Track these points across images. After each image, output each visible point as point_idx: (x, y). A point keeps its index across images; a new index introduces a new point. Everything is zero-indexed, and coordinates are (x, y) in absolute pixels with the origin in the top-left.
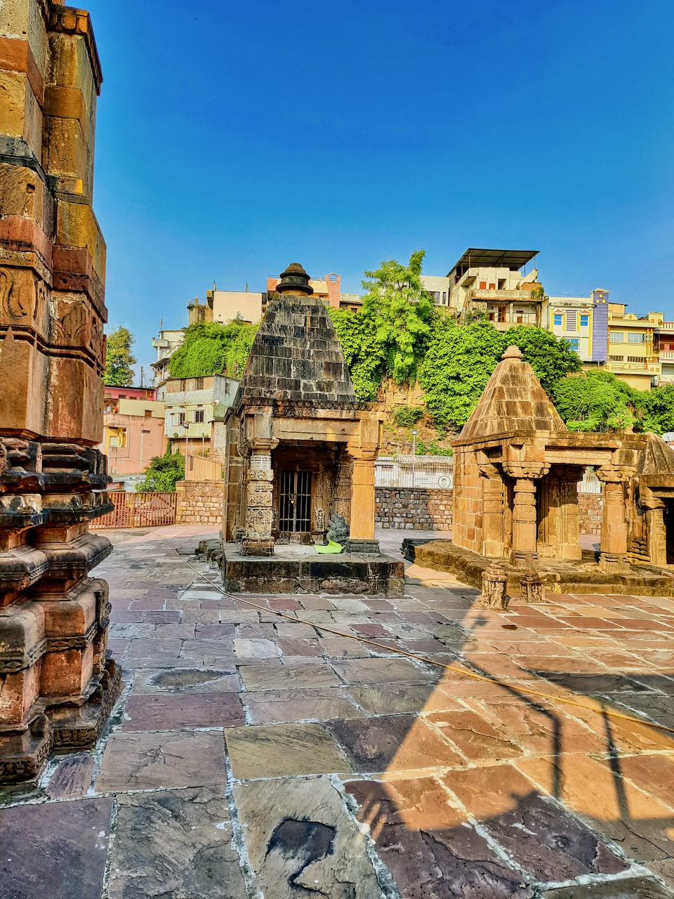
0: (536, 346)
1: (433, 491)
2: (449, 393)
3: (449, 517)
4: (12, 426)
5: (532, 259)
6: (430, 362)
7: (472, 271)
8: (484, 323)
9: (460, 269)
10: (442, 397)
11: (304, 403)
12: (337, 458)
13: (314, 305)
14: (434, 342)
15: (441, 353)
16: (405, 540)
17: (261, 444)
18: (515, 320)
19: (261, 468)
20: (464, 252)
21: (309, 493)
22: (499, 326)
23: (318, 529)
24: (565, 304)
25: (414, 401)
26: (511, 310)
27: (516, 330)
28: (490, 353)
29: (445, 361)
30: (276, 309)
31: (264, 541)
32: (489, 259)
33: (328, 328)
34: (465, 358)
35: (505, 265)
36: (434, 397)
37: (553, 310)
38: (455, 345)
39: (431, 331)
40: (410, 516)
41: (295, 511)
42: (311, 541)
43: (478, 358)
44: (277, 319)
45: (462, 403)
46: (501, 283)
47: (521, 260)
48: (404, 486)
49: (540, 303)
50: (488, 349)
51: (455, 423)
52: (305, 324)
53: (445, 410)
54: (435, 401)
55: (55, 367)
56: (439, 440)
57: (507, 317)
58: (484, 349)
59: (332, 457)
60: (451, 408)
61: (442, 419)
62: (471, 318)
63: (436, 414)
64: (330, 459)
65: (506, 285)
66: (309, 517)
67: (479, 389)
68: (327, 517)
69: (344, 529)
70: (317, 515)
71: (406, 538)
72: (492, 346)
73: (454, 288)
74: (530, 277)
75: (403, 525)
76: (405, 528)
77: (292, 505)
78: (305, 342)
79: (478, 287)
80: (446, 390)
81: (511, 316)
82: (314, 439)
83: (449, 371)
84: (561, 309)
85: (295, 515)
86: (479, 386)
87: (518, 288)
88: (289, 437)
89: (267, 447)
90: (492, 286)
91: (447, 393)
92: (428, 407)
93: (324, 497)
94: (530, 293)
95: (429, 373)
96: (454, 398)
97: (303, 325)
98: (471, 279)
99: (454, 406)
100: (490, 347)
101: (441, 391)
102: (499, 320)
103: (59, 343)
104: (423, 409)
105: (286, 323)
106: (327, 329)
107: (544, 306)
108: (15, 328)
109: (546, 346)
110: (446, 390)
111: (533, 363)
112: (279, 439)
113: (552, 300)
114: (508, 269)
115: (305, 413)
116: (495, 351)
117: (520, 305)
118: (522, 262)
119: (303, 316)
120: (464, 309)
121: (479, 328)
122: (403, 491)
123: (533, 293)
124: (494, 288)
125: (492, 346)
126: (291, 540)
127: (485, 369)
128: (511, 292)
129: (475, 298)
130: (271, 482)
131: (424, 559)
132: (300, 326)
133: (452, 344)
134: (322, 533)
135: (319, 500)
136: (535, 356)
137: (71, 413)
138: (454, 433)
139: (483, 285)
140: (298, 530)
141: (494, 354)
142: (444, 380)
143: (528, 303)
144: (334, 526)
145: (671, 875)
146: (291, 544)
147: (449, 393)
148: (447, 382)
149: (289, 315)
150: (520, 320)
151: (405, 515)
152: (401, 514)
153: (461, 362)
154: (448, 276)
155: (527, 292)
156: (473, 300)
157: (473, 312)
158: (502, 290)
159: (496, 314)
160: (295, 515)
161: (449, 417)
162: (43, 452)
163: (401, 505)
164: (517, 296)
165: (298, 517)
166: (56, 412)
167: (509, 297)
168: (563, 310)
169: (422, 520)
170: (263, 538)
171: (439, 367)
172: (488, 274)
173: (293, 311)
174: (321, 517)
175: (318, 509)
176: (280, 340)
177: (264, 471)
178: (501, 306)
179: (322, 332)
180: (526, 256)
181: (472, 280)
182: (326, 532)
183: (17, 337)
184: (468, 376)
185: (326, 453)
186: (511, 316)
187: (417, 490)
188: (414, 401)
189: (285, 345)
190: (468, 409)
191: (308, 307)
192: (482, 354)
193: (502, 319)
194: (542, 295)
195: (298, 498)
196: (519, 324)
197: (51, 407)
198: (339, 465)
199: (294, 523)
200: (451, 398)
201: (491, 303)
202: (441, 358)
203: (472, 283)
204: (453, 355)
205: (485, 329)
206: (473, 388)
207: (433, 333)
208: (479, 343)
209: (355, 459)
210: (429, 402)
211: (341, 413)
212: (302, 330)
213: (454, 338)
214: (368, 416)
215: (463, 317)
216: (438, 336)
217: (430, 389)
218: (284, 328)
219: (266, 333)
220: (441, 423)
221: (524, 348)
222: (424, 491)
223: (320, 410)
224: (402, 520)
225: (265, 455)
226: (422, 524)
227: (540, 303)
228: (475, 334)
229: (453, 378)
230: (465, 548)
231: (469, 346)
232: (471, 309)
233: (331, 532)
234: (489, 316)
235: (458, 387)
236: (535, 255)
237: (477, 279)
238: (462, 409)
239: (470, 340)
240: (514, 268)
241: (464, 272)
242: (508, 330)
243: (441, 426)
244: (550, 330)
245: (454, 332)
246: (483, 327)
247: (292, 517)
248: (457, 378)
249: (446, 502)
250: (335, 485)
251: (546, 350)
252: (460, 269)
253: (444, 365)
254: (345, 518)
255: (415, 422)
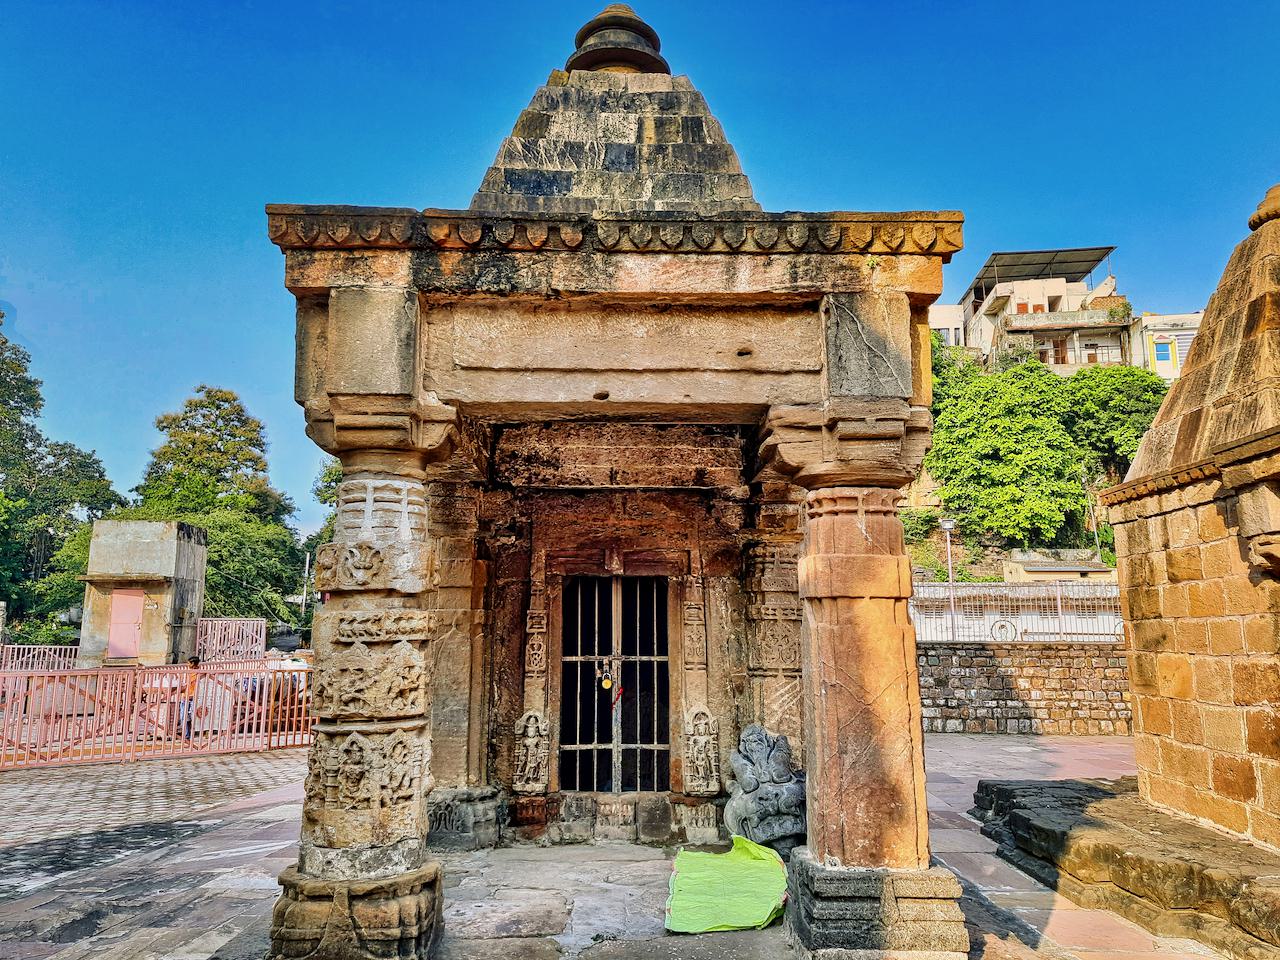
0: (1130, 397)
1: (1000, 647)
2: (983, 482)
3: (1043, 704)
5: (1101, 264)
6: (943, 434)
7: (1001, 289)
8: (1034, 365)
9: (980, 291)
10: (971, 489)
11: (554, 230)
12: (749, 524)
13: (671, 90)
14: (947, 401)
15: (962, 417)
17: (360, 420)
18: (1085, 360)
19: (367, 535)
20: (986, 259)
21: (663, 651)
22: (1060, 372)
23: (693, 784)
24: (1174, 325)
25: (922, 501)
26: (1077, 344)
27: (1088, 374)
28: (1049, 413)
29: (971, 429)
30: (554, 106)
31: (369, 896)
32: (1028, 269)
33: (709, 142)
34: (1006, 422)
35: (1056, 275)
36: (956, 492)
37: (1151, 338)
38: (985, 403)
39: (942, 385)
40: (954, 703)
42: (674, 827)
43: (1029, 420)
44: (554, 129)
45: (1008, 497)
46: (1053, 303)
47: (1083, 266)
48: (934, 639)
49: (1126, 328)
50: (1045, 406)
51: (999, 533)
52: (639, 138)
53: (980, 512)
54: (959, 497)
56: (972, 563)
57: (1070, 355)
58: (1038, 406)
59: (733, 519)
60: (987, 507)
61: (974, 527)
62: (1007, 361)
63: (963, 520)
64: (726, 531)
65: (1063, 306)
66: (664, 738)
67: (1035, 473)
68: (726, 739)
69: (787, 790)
70: (690, 729)
71: (990, 776)
72: (1052, 400)
73: (973, 320)
74: (1104, 289)
75: (939, 723)
76: (944, 731)
77: (606, 695)
78: (639, 181)
79: (1015, 311)
80: (977, 478)
81: (1078, 352)
82: (612, 398)
83: (980, 445)
84: (1166, 334)
85: (616, 729)
86: (1035, 467)
87: (1083, 307)
89: (390, 438)
90: (1038, 308)
91: (979, 484)
92: (947, 509)
93: (713, 663)
94: (1107, 313)
95: (944, 452)
96: (992, 490)
97: (632, 139)
98: (1001, 301)
99: (994, 503)
100: (1048, 402)
101: (969, 480)
102: (1057, 362)
104: (938, 512)
105: (585, 137)
106: (705, 145)
107: (1135, 333)
109: (1149, 396)
110: (977, 478)
111: (1127, 425)
113: (1147, 320)
114: (1064, 279)
115: (561, 273)
116: (1057, 409)
117: (1092, 335)
118: (1096, 258)
119: (632, 117)
120: (994, 348)
121: (1025, 372)
122: (934, 649)
123: (1112, 314)
124: (1043, 311)
125: (1052, 400)
126: (598, 826)
127: (1042, 438)
128: (1073, 314)
129: (1010, 329)
131: (1082, 873)
132: (625, 142)
133: (980, 402)
134: (711, 798)
135: (696, 677)
136: (1130, 413)
138: (997, 550)
139: (1022, 308)
140: (628, 784)
141: (1057, 414)
142: (971, 461)
143: (1104, 330)
144: (748, 774)
146: (600, 841)
147: (983, 482)
148: (978, 464)
149: (590, 116)
150: (1092, 358)
151: (942, 702)
152: (933, 699)
153: (999, 430)
154: (960, 304)
155: (1101, 313)
156: (1009, 332)
157: (1010, 351)
158: (1056, 314)
159: (1051, 353)
160: (616, 729)
161: (986, 524)
163: (931, 680)
164: (1084, 320)
165: (627, 738)
167: (1071, 323)
168: (1171, 336)
169: (982, 712)
170: (366, 880)
171: (960, 441)
172: (1031, 291)
173: (604, 106)
174: (702, 740)
175: (695, 705)
176: (561, 181)
177: (378, 545)
178: (1059, 338)
179: (690, 154)
180: (1092, 258)
181: (1004, 301)
182: (723, 795)
184: (1014, 452)
185: (709, 509)
186: (1078, 352)
187: (964, 646)
188: (922, 501)
189: (577, 192)
190: (1019, 507)
191: (649, 95)
192: (1034, 415)
193: (1061, 360)
194: (1129, 315)
195: (628, 668)
196: (1093, 365)
198: (759, 550)
199: (617, 760)
200: (988, 490)
201: (1039, 334)
202: (963, 425)
203: (1002, 308)
204: (983, 420)
205: (1035, 374)
206: (1025, 471)
207: (945, 388)
208: (1028, 398)
209: (812, 482)
210: (949, 501)
211: (731, 273)
212: (631, 153)
213: (983, 392)
214: (856, 279)
215: (992, 361)
216: (954, 392)
217: (948, 479)
218: (573, 150)
219: (518, 165)
220: (974, 533)
221: (1107, 402)
222: (983, 647)
223: (631, 262)
224: (937, 712)
225: (387, 474)
226: (982, 721)
227: (1126, 328)
228: (1019, 383)
229: (987, 456)
230: (1205, 823)
231: (1013, 403)
232: (1006, 346)
233: (739, 803)
234: (1038, 355)
235: (997, 471)
236: (1107, 253)
237: (1012, 299)
238: (1010, 507)
239: (1012, 394)
240: (1072, 278)
241: (987, 294)
242: (1074, 375)
243: (974, 539)
244: (1150, 369)
245: (984, 381)
246: (1032, 371)
247: (606, 737)
248: (995, 456)
249: (1031, 671)
250: (750, 621)
251: (1149, 402)
252: (980, 291)
253: (970, 437)
254: (793, 742)
255: (927, 534)
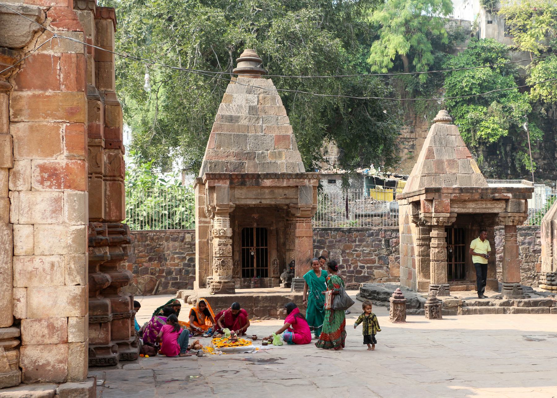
4: (96, 217)
16: (200, 287)
21: (266, 245)
41: (255, 260)
55: (108, 186)
88: (243, 202)
89: (226, 211)
103: (109, 174)
108: (96, 173)
112: (236, 204)
130: (231, 238)
137: (116, 208)
145: (5, 17)
162: (108, 227)
166: (109, 208)
183: (97, 177)
197: (107, 206)
